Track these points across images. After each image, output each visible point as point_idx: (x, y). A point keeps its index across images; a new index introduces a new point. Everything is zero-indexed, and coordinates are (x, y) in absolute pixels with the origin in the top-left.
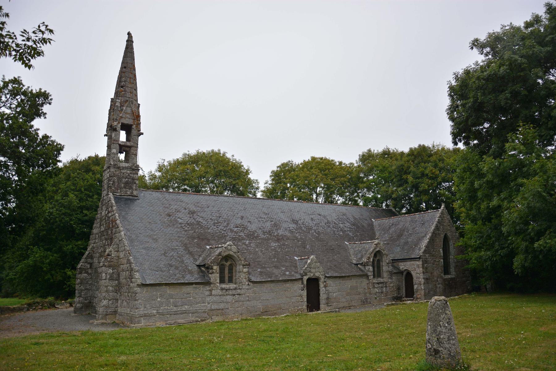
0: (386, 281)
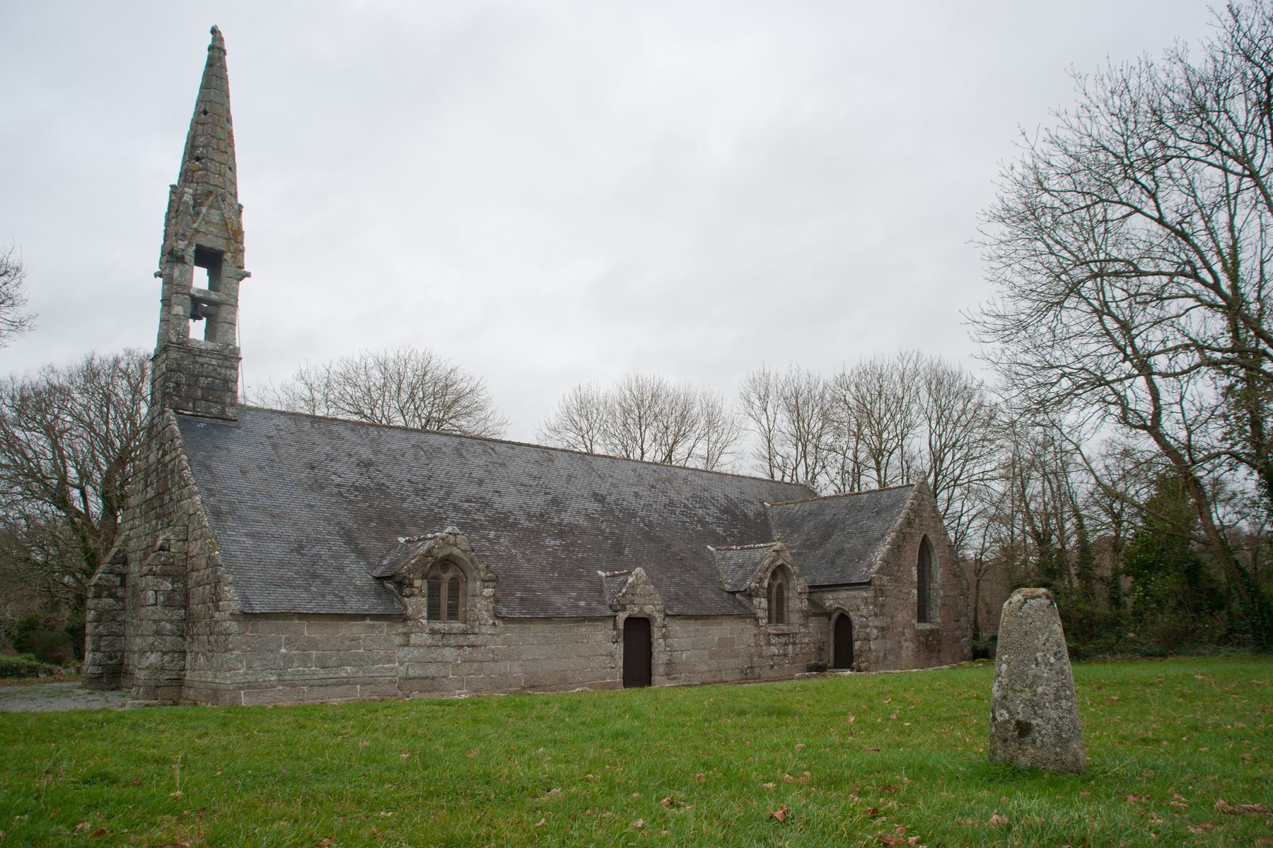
0: (794, 631)
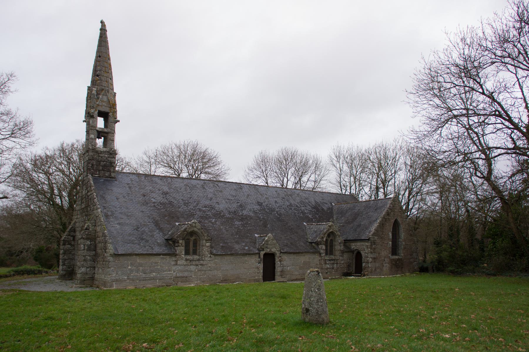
0: (337, 258)
